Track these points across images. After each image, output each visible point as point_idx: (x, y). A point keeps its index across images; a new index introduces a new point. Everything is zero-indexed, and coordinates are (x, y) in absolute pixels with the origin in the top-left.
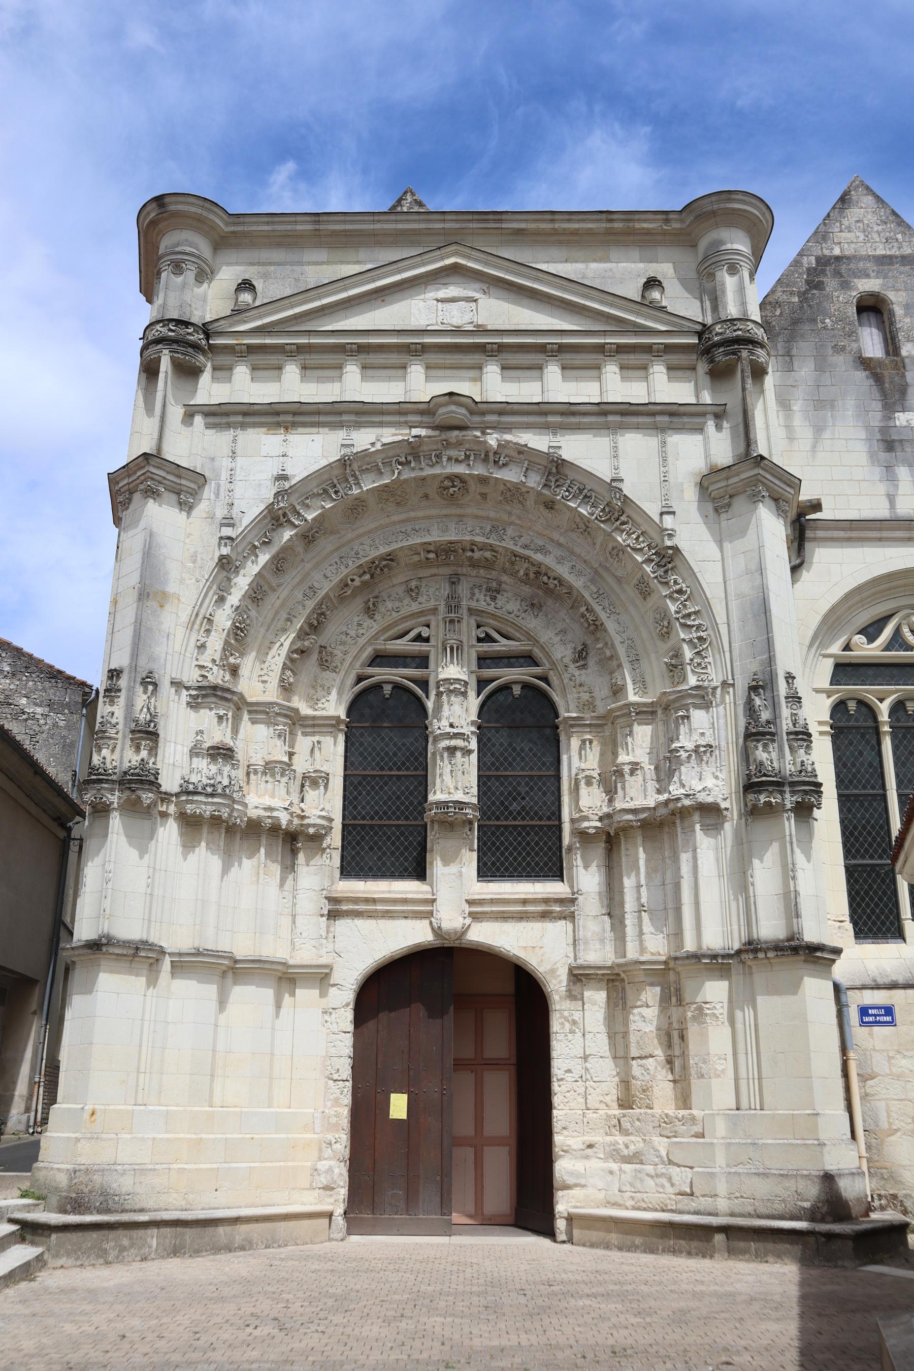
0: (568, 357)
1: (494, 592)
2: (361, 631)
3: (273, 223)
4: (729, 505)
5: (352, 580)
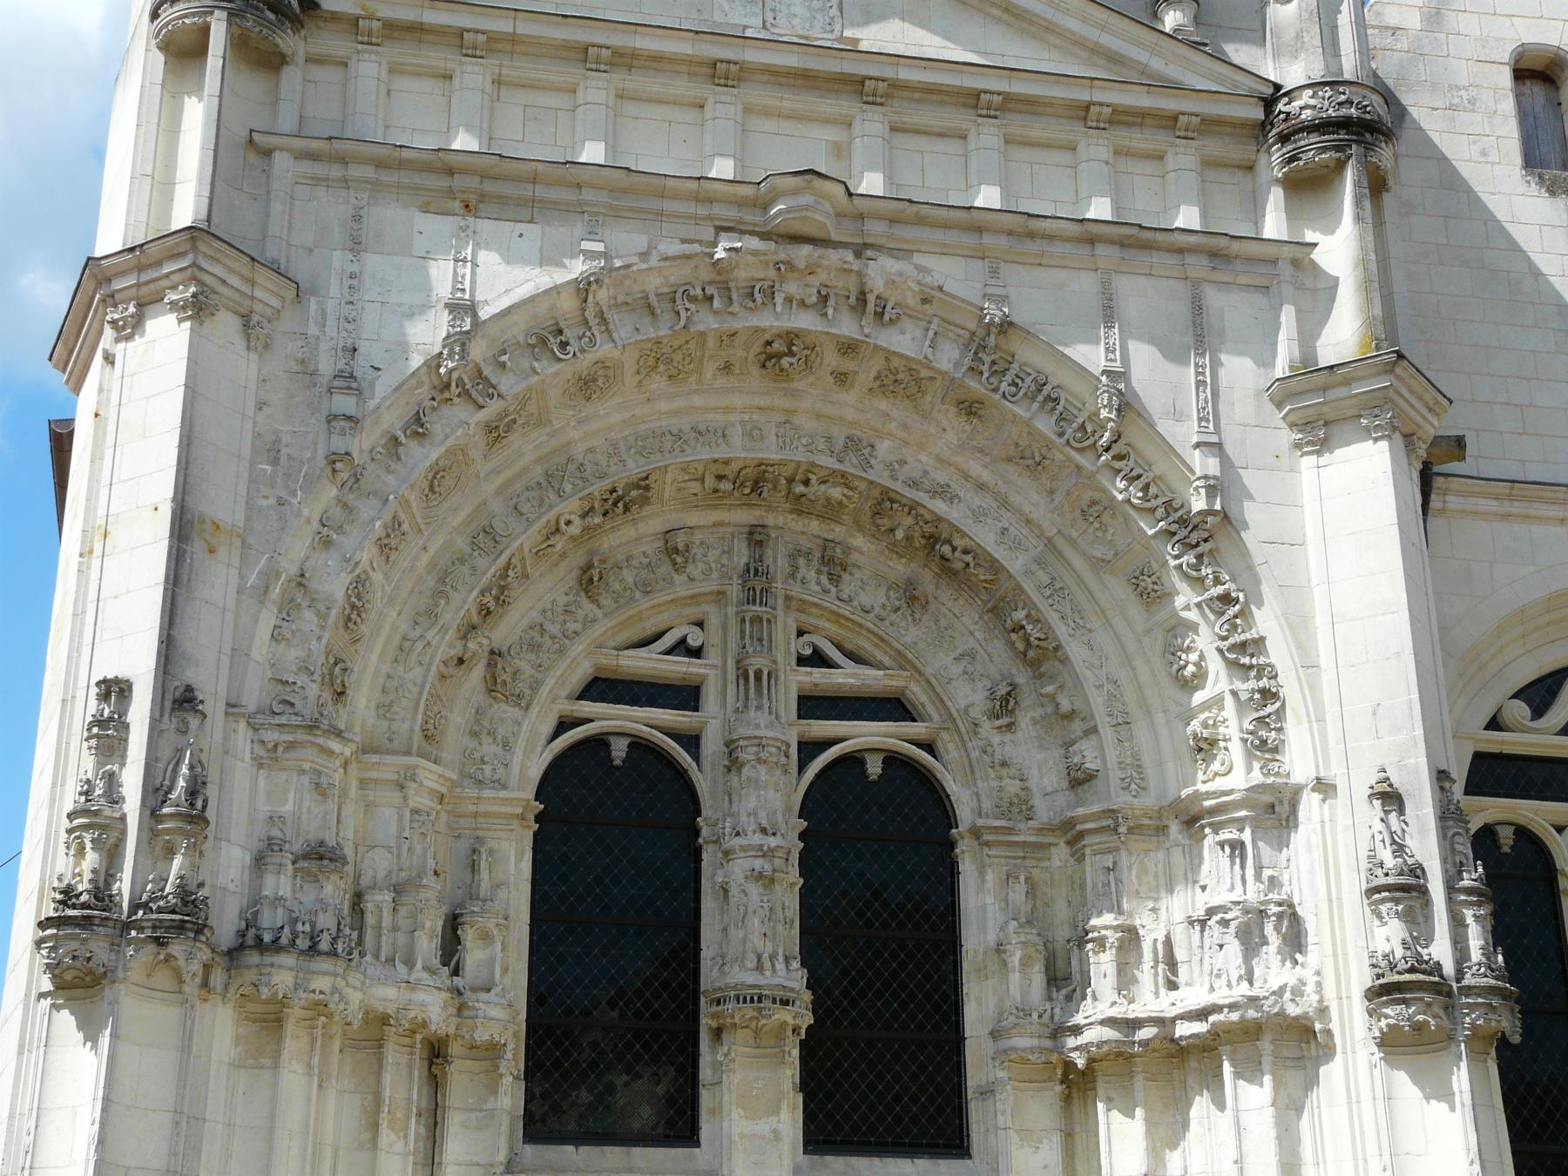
0: (1017, 123)
2: (572, 627)
5: (568, 523)
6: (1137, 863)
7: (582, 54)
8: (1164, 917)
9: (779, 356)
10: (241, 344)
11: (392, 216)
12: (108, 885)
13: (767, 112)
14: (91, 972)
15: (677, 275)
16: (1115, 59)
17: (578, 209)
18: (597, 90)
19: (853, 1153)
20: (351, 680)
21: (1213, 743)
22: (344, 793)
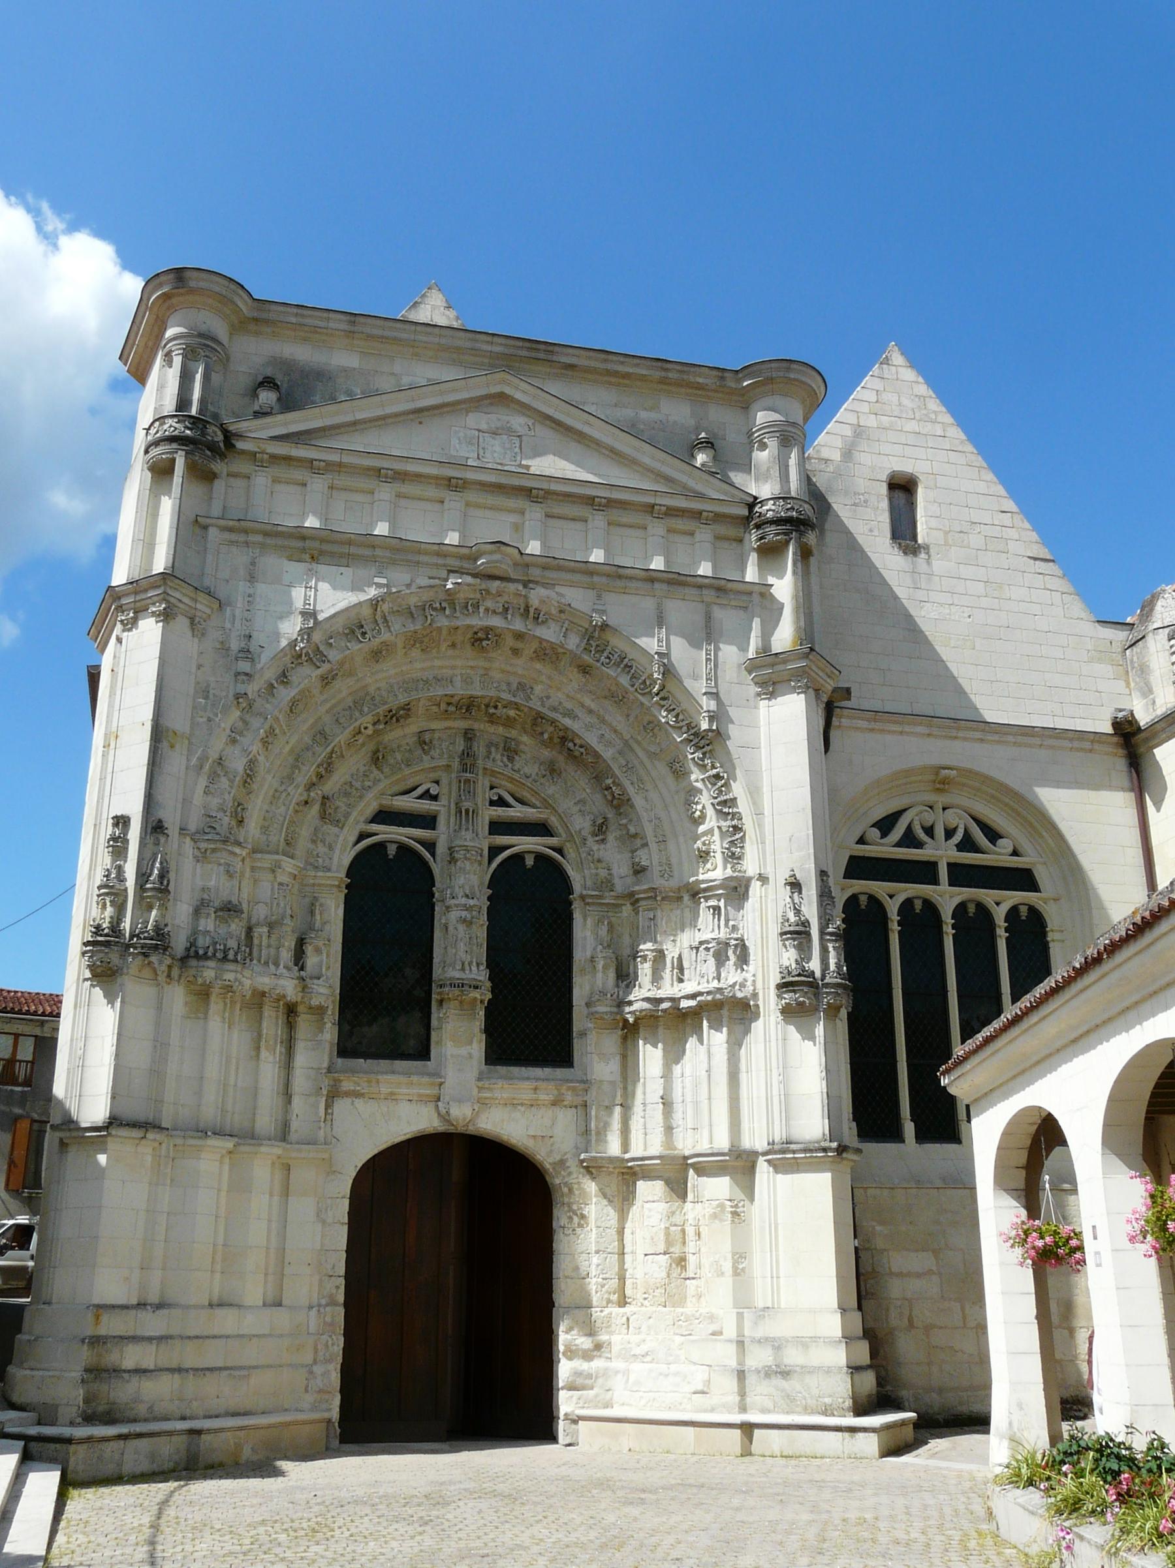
0: (615, 514)
2: (367, 784)
3: (303, 316)
5: (366, 728)
6: (666, 915)
7: (377, 472)
8: (677, 946)
9: (481, 639)
10: (189, 634)
11: (272, 562)
12: (118, 924)
13: (478, 506)
14: (110, 969)
15: (426, 596)
16: (669, 480)
17: (373, 560)
18: (385, 492)
19: (521, 1065)
20: (246, 814)
21: (707, 853)
22: (242, 874)
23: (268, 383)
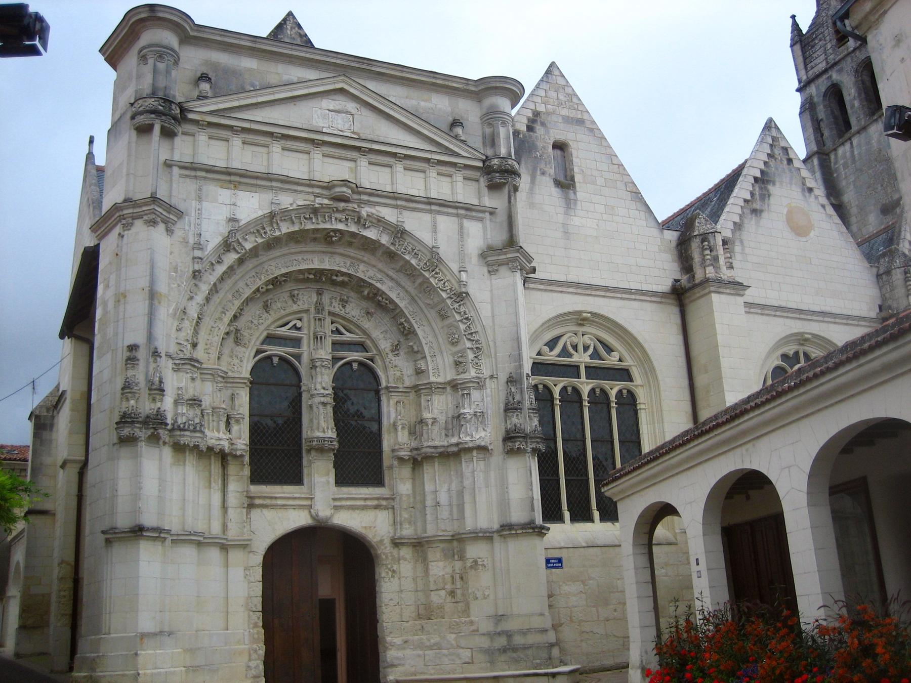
1: (344, 302)
2: (261, 321)
4: (497, 270)
10: (165, 233)
23: (204, 77)
